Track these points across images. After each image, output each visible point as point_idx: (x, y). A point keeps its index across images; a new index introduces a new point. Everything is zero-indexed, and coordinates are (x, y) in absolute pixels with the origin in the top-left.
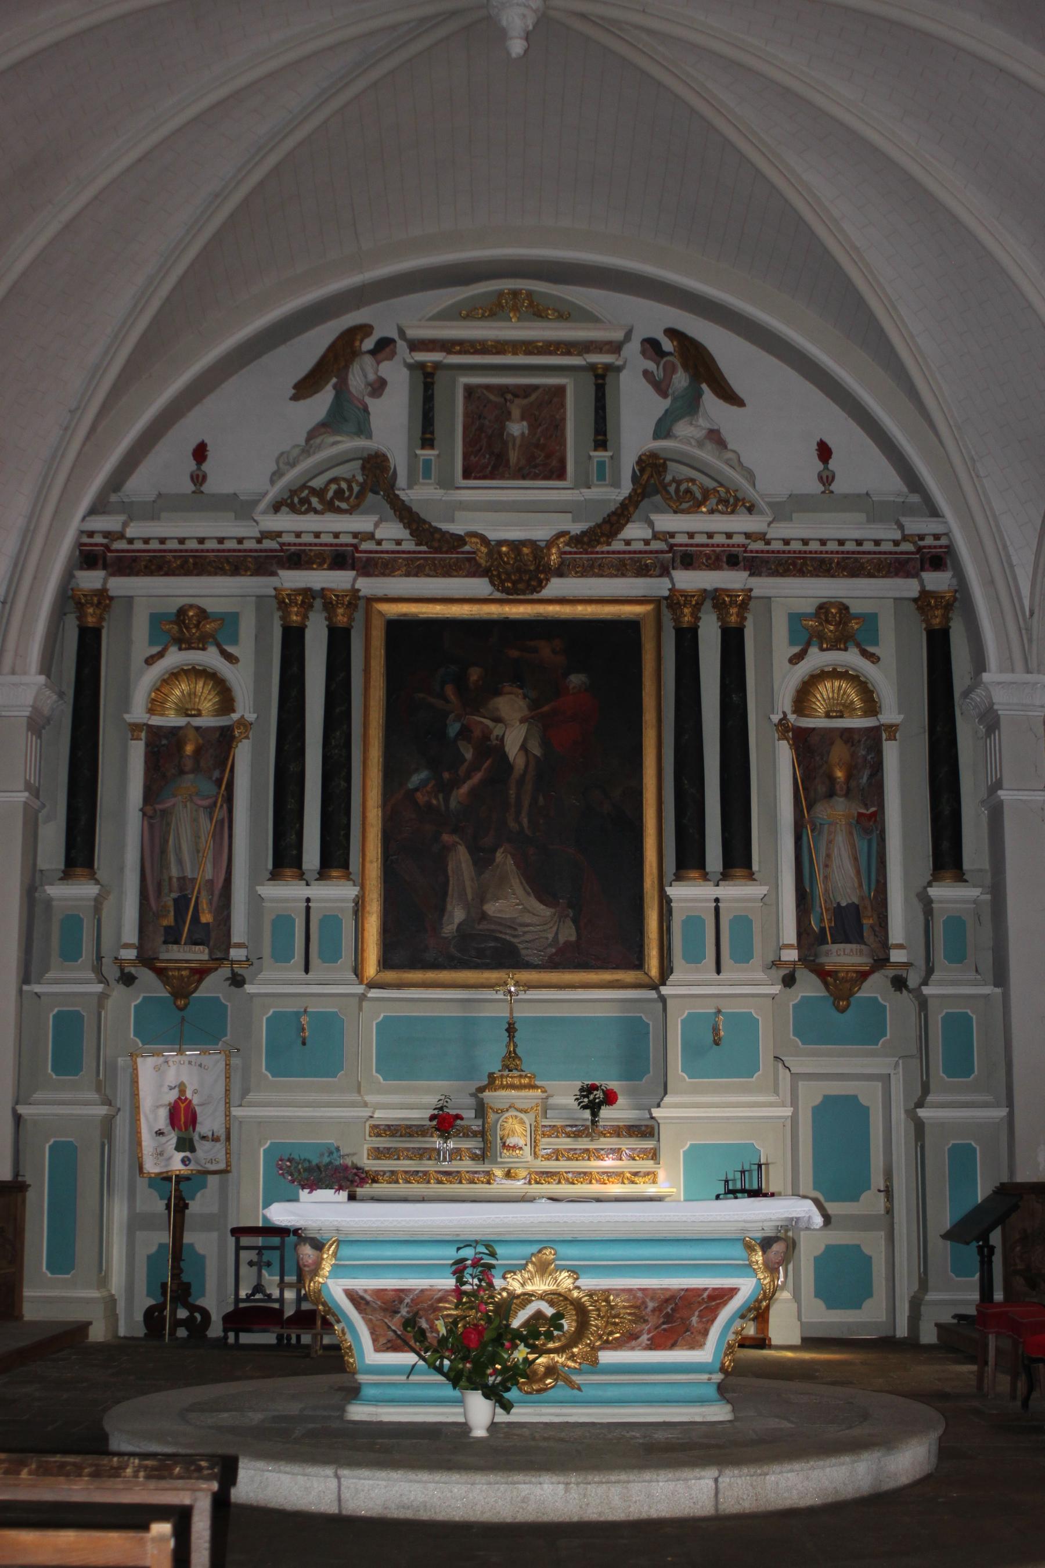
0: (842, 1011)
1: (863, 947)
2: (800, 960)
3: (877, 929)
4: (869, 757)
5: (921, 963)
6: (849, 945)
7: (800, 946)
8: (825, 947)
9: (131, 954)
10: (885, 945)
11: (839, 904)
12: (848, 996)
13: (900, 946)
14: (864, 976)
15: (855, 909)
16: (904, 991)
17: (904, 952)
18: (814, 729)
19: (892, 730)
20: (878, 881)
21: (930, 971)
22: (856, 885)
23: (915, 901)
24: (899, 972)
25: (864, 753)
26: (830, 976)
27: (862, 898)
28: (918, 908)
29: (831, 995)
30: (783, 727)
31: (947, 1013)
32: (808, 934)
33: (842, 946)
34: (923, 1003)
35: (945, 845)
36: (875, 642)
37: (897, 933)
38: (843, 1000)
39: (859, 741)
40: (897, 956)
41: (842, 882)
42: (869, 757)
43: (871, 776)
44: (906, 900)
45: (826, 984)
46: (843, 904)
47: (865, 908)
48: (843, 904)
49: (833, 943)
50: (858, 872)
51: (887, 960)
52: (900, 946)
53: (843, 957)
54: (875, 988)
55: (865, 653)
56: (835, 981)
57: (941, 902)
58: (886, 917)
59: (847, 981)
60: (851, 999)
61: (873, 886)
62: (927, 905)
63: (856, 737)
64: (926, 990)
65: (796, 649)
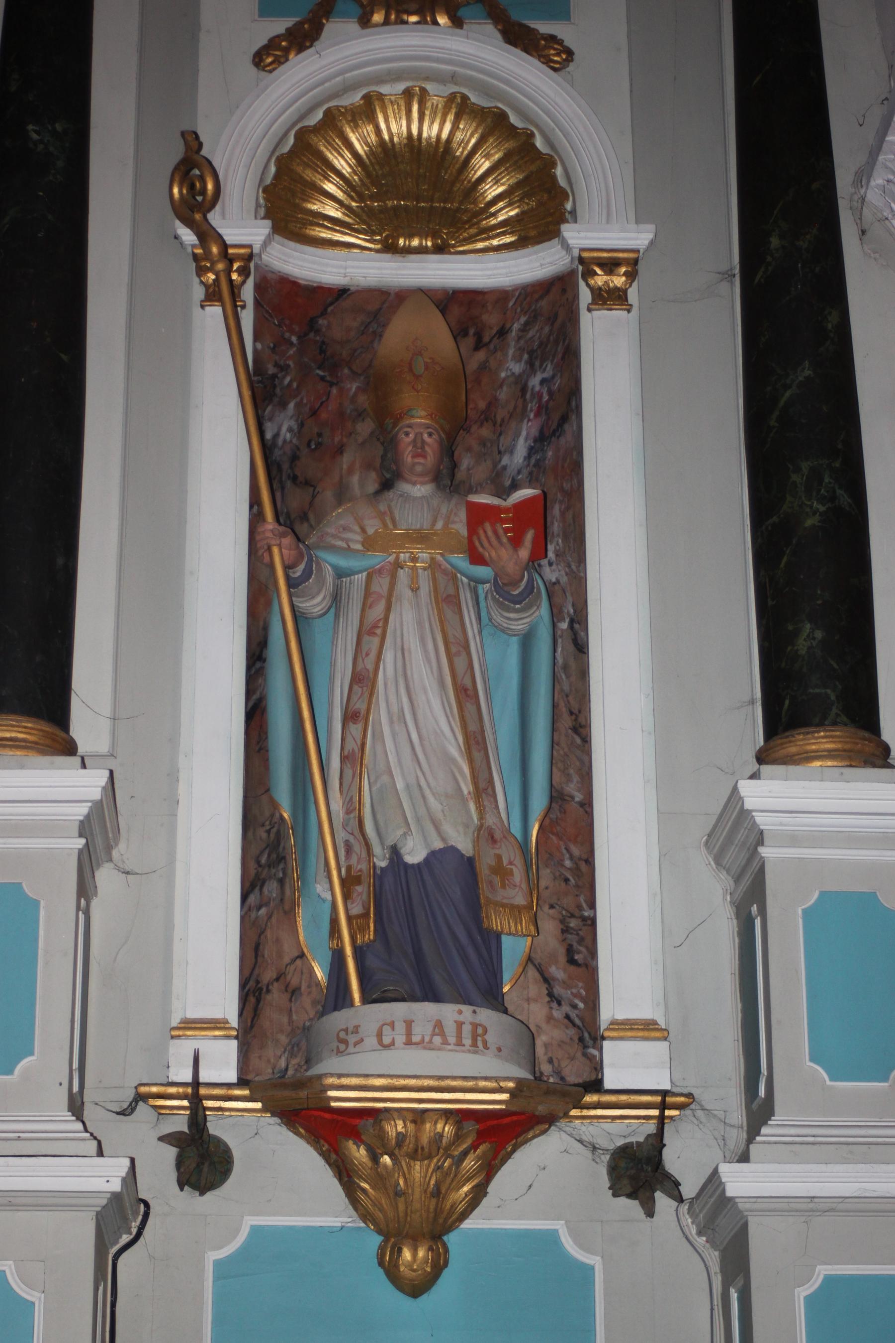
0: (416, 1289)
1: (486, 1016)
2: (242, 1082)
3: (557, 972)
4: (535, 382)
5: (726, 1097)
6: (429, 1009)
7: (250, 1031)
8: (339, 1019)
9: (221, 1062)
10: (588, 1034)
11: (395, 852)
12: (437, 1228)
13: (645, 1029)
14: (498, 1134)
15: (460, 876)
16: (662, 1200)
17: (658, 1049)
18: (342, 292)
19: (611, 276)
20: (557, 797)
21: (759, 1113)
22: (467, 788)
23: (701, 863)
24: (696, 1237)
25: (517, 368)
26: (357, 1137)
27: (488, 836)
28: (715, 893)
29: (365, 1216)
30: (222, 271)
31: (829, 1280)
32: (294, 993)
33: (399, 1010)
34: (728, 1233)
35: (808, 637)
36: (560, 8)
37: (630, 972)
38: (415, 1241)
39: (503, 332)
40: (628, 1066)
41: (417, 782)
42: (535, 382)
43: (542, 440)
44: (668, 857)
45: (344, 1172)
46: (414, 854)
47: (501, 871)
48: (414, 854)
49: (367, 999)
50: (475, 742)
51: (596, 1085)
52: (645, 1029)
53: (413, 1061)
54: (546, 1188)
55: (518, 36)
56: (375, 1158)
57: (794, 840)
58: (591, 923)
59: (416, 1154)
60: (452, 1239)
61: (539, 802)
62: (738, 847)
63: (491, 319)
64: (739, 1182)
65: (279, 26)
